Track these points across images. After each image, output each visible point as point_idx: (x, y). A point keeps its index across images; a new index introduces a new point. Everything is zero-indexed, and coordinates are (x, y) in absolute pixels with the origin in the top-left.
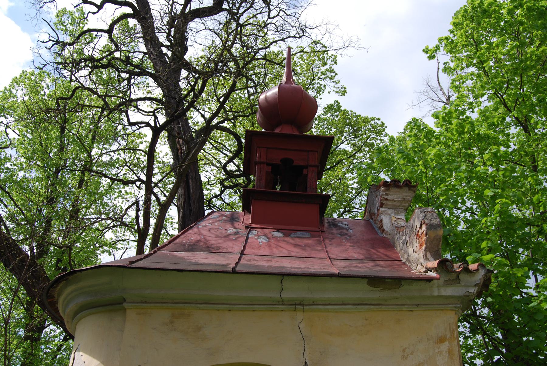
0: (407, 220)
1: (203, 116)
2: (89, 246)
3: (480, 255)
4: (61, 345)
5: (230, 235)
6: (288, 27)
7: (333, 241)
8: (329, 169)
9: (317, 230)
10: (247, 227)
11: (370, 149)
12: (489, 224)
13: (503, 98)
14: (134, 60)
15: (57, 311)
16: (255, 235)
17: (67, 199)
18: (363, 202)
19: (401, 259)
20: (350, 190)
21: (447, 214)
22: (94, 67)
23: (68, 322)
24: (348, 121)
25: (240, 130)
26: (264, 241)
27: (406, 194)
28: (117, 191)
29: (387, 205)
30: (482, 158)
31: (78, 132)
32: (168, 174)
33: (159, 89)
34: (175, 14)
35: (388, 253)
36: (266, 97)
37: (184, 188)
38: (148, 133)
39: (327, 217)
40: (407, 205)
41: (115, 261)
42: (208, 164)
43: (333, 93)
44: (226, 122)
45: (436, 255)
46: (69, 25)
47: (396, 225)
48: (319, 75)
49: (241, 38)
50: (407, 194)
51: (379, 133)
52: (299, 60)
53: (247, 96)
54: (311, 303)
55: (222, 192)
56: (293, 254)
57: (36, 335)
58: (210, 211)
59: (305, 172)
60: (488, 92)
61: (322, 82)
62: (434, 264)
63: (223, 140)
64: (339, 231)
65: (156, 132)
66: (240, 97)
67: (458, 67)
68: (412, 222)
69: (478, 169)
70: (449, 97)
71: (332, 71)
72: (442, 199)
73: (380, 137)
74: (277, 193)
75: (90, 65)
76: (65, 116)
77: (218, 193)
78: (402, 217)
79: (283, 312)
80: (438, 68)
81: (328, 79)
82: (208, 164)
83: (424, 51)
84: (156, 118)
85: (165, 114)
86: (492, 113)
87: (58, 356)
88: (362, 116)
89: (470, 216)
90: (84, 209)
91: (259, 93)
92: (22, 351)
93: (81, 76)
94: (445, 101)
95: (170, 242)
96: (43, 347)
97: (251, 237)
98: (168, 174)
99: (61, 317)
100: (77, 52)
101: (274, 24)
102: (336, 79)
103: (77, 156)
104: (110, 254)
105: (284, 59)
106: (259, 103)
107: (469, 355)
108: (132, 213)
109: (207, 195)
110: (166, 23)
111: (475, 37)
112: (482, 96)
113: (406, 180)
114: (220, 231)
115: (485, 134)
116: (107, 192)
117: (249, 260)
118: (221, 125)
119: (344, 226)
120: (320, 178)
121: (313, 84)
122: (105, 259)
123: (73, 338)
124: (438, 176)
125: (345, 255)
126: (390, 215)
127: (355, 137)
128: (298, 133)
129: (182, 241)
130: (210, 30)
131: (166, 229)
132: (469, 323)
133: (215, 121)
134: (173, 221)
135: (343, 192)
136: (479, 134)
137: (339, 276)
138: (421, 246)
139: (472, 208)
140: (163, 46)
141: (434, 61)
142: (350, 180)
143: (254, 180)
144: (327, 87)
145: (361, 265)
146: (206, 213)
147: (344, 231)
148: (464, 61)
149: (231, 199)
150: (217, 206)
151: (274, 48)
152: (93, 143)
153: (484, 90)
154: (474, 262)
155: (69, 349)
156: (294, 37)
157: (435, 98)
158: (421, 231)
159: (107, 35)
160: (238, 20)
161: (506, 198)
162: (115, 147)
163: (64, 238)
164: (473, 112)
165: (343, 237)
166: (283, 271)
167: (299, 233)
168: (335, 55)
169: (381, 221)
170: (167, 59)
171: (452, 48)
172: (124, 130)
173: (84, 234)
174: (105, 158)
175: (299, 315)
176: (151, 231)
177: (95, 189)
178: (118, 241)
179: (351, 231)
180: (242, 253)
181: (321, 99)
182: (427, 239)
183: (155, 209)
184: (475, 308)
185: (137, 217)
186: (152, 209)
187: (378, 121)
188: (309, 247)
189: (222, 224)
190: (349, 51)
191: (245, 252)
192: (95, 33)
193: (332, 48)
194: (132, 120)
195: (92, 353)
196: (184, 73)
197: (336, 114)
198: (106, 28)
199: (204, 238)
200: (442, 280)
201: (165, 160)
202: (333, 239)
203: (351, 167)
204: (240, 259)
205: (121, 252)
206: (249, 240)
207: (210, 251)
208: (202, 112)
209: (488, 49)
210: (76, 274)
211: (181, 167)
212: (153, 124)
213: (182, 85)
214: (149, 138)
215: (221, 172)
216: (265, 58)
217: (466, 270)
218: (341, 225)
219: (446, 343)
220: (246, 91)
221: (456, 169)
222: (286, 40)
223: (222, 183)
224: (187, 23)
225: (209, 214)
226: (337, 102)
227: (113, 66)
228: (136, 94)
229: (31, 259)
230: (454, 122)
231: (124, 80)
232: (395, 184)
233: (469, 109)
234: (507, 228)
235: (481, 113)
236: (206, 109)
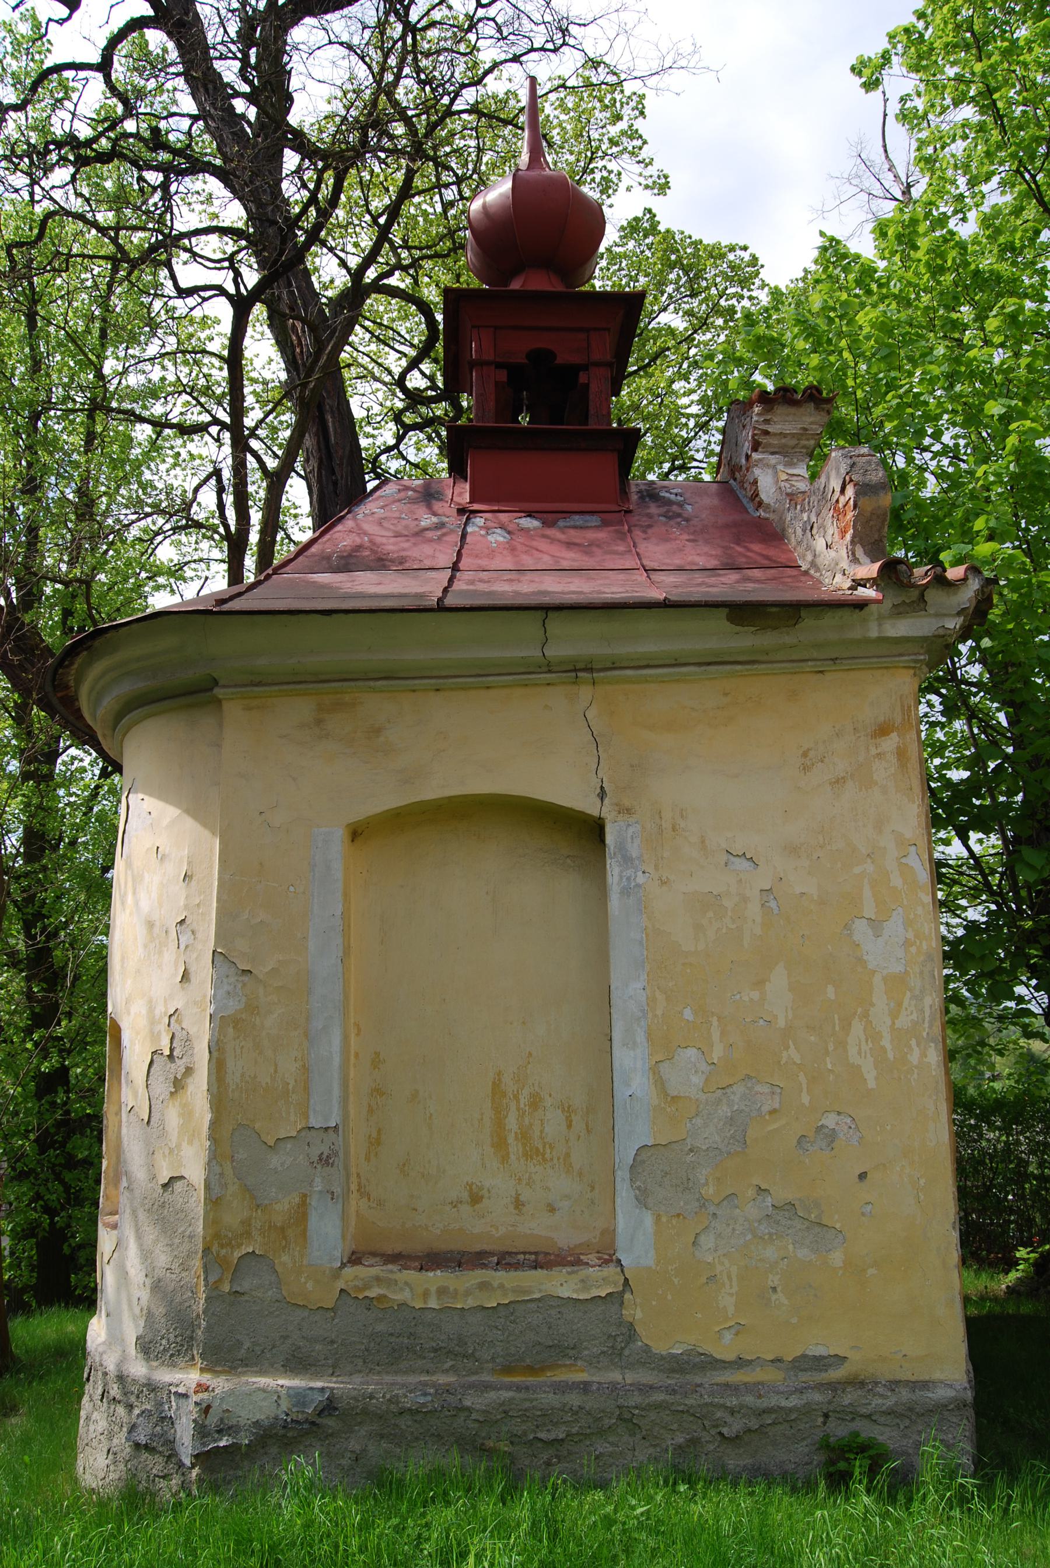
0: (814, 477)
1: (343, 264)
2: (126, 580)
3: (970, 547)
4: (97, 787)
5: (427, 529)
6: (527, 25)
7: (650, 531)
8: (635, 372)
9: (616, 508)
10: (461, 511)
11: (726, 322)
12: (992, 478)
13: (1035, 182)
14: (172, 137)
15: (81, 717)
16: (481, 528)
17: (64, 478)
18: (713, 446)
19: (800, 563)
20: (684, 420)
21: (900, 462)
22: (81, 162)
23: (104, 736)
24: (673, 257)
25: (431, 294)
26: (501, 539)
27: (809, 419)
28: (169, 452)
30: (983, 329)
31: (67, 322)
32: (279, 403)
33: (237, 201)
34: (255, 10)
35: (771, 552)
36: (484, 206)
37: (317, 434)
38: (222, 310)
39: (634, 486)
40: (812, 442)
41: (184, 603)
42: (364, 377)
43: (638, 190)
44: (397, 273)
45: (874, 550)
46: (8, 57)
47: (789, 491)
48: (604, 147)
49: (415, 60)
50: (812, 419)
51: (745, 282)
52: (556, 113)
53: (439, 208)
54: (609, 665)
55: (400, 439)
56: (565, 564)
57: (45, 769)
58: (377, 482)
59: (583, 378)
60: (1002, 169)
61: (613, 166)
62: (870, 569)
63: (393, 320)
64: (663, 510)
65: (241, 306)
66: (425, 213)
67: (933, 106)
68: (823, 480)
69: (971, 354)
70: (909, 186)
71: (633, 134)
72: (888, 426)
73: (749, 290)
74: (524, 430)
75: (71, 158)
76: (31, 284)
77: (392, 442)
78: (802, 470)
79: (550, 688)
80: (885, 115)
81: (626, 156)
82: (364, 377)
83: (853, 69)
84: (237, 274)
85: (255, 266)
86: (1008, 221)
87: (95, 810)
88: (705, 242)
89: (950, 464)
90: (104, 499)
91: (467, 199)
92: (22, 802)
93: (53, 187)
94: (898, 195)
95: (298, 554)
96: (61, 792)
97: (473, 533)
98: (279, 403)
99: (89, 726)
100: (34, 129)
101: (493, 20)
102: (644, 154)
103: (72, 380)
104: (173, 592)
105: (522, 110)
106: (468, 218)
107: (937, 761)
108: (208, 498)
109: (367, 450)
110: (233, 35)
111: (976, 28)
112: (987, 179)
113: (811, 387)
114: (404, 523)
115: (991, 272)
116: (147, 456)
117: (472, 582)
118: (385, 281)
119: (673, 497)
120: (617, 394)
121: (592, 171)
122: (160, 601)
123: (118, 769)
124: (881, 375)
125: (677, 562)
126: (774, 467)
127: (693, 295)
128: (560, 288)
129: (323, 551)
130: (341, 44)
131: (284, 530)
132: (940, 695)
133: (371, 274)
134: (298, 511)
135: (669, 423)
136: (977, 273)
137: (666, 605)
138: (843, 533)
139: (957, 445)
140: (237, 94)
141: (876, 95)
142: (684, 394)
143: (469, 408)
144: (623, 176)
145: (713, 580)
146: (370, 486)
147: (675, 508)
148: (948, 90)
149: (421, 455)
150: (392, 471)
151: (494, 85)
152: (103, 345)
153: (992, 163)
154: (957, 562)
155: (113, 791)
156: (543, 49)
157: (877, 190)
158: (843, 500)
159: (99, 76)
160: (407, 14)
161: (1033, 421)
162: (153, 350)
163: (71, 563)
164: (964, 220)
165: (672, 523)
166: (546, 600)
167: (577, 517)
168: (640, 92)
169: (755, 482)
170: (248, 130)
171: (920, 57)
172: (167, 312)
173: (111, 553)
174: (133, 380)
175: (585, 692)
176: (254, 537)
177: (123, 452)
178: (186, 563)
179: (689, 508)
180: (455, 568)
181: (611, 206)
182: (857, 519)
183: (257, 488)
184: (953, 663)
185: (221, 506)
186: (251, 489)
187: (742, 254)
188: (598, 546)
189: (405, 508)
190: (674, 80)
191: (461, 566)
192: (69, 74)
193: (635, 74)
194: (184, 284)
195: (162, 794)
196: (291, 159)
197: (647, 241)
198: (95, 58)
199: (371, 541)
200: (888, 604)
201: (268, 375)
202: (650, 526)
203: (685, 366)
204: (451, 580)
205: (198, 584)
206: (469, 539)
207: (385, 568)
208: (342, 255)
209: (1006, 53)
210: (107, 636)
211: (304, 386)
212: (231, 289)
213: (288, 188)
214: (226, 327)
215: (394, 394)
216: (474, 109)
217: (941, 581)
218: (667, 495)
219: (894, 735)
220: (437, 198)
221: (924, 355)
222: (524, 59)
223: (397, 418)
224: (286, 30)
225: (376, 489)
226: (650, 211)
227: (123, 157)
228: (185, 220)
229: (8, 613)
230: (923, 243)
231: (155, 189)
232: (785, 396)
233: (956, 212)
234: (1031, 488)
235: (986, 221)
236: (350, 248)
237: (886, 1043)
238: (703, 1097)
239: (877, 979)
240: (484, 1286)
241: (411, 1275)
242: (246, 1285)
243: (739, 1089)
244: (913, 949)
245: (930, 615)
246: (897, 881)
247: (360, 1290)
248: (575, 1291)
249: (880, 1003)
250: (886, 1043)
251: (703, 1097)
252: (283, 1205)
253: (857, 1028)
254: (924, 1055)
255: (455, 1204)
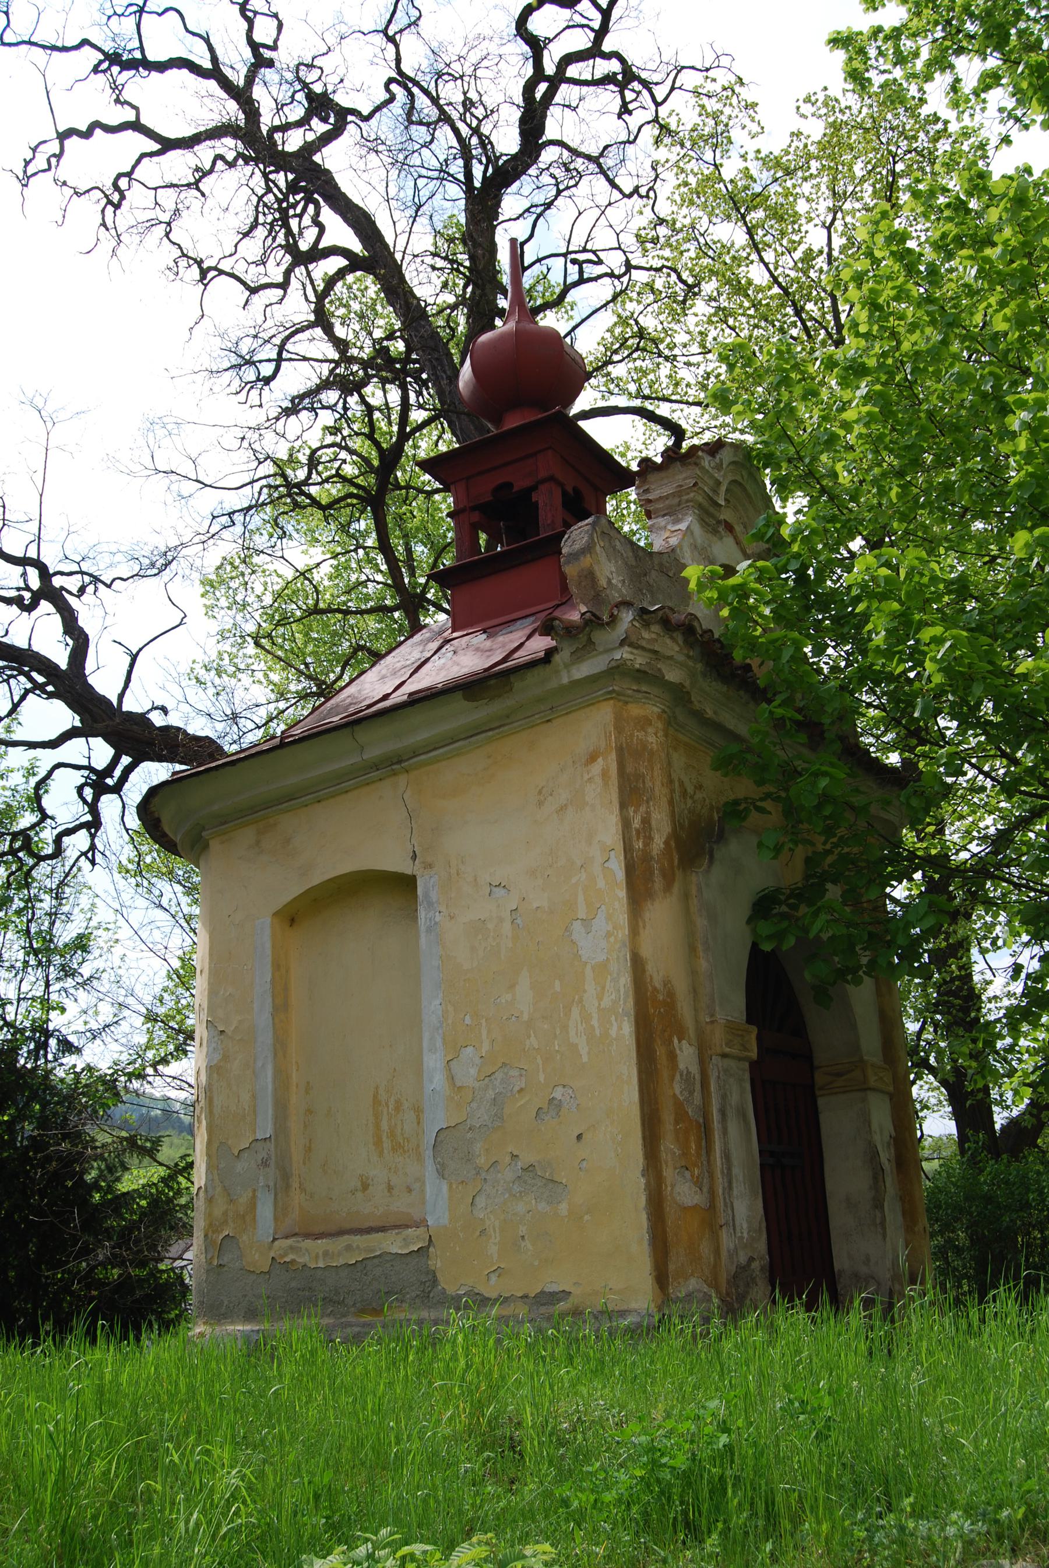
29: (657, 511)
219: (600, 760)
237: (595, 1022)
238: (477, 1085)
239: (588, 970)
240: (348, 1248)
241: (308, 1243)
242: (225, 1260)
243: (499, 1075)
244: (612, 939)
245: (601, 653)
246: (601, 884)
247: (282, 1256)
248: (401, 1248)
249: (591, 988)
250: (595, 1022)
251: (477, 1085)
252: (244, 1199)
253: (575, 1012)
254: (620, 1028)
255: (353, 1193)
